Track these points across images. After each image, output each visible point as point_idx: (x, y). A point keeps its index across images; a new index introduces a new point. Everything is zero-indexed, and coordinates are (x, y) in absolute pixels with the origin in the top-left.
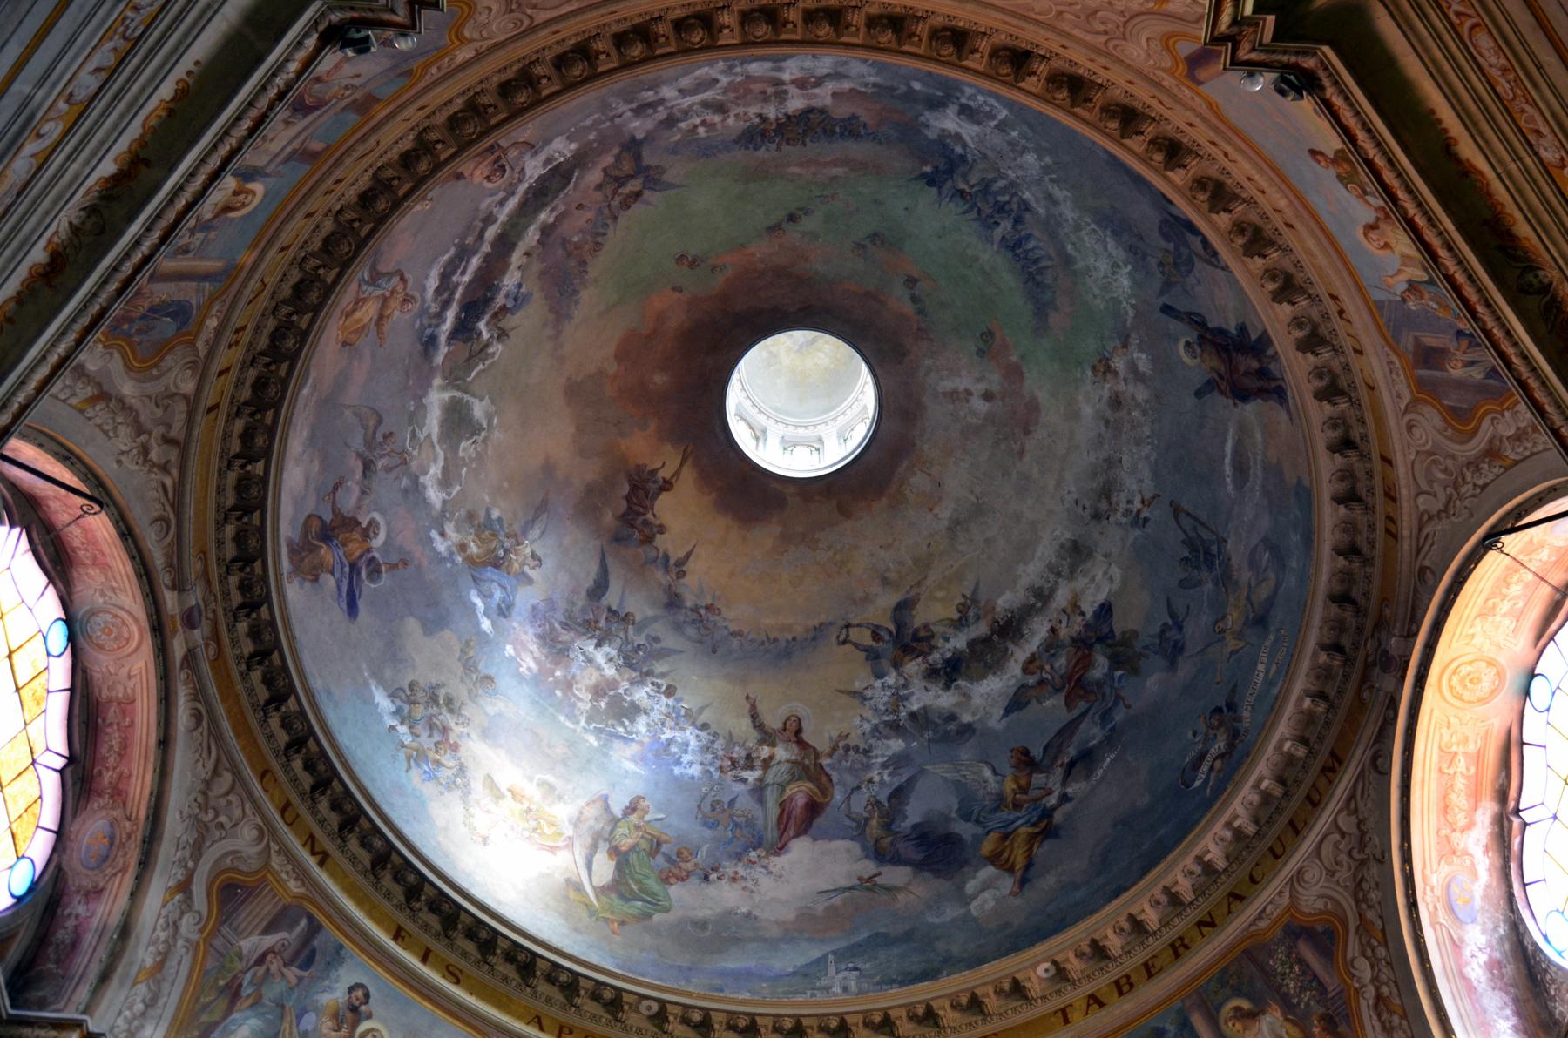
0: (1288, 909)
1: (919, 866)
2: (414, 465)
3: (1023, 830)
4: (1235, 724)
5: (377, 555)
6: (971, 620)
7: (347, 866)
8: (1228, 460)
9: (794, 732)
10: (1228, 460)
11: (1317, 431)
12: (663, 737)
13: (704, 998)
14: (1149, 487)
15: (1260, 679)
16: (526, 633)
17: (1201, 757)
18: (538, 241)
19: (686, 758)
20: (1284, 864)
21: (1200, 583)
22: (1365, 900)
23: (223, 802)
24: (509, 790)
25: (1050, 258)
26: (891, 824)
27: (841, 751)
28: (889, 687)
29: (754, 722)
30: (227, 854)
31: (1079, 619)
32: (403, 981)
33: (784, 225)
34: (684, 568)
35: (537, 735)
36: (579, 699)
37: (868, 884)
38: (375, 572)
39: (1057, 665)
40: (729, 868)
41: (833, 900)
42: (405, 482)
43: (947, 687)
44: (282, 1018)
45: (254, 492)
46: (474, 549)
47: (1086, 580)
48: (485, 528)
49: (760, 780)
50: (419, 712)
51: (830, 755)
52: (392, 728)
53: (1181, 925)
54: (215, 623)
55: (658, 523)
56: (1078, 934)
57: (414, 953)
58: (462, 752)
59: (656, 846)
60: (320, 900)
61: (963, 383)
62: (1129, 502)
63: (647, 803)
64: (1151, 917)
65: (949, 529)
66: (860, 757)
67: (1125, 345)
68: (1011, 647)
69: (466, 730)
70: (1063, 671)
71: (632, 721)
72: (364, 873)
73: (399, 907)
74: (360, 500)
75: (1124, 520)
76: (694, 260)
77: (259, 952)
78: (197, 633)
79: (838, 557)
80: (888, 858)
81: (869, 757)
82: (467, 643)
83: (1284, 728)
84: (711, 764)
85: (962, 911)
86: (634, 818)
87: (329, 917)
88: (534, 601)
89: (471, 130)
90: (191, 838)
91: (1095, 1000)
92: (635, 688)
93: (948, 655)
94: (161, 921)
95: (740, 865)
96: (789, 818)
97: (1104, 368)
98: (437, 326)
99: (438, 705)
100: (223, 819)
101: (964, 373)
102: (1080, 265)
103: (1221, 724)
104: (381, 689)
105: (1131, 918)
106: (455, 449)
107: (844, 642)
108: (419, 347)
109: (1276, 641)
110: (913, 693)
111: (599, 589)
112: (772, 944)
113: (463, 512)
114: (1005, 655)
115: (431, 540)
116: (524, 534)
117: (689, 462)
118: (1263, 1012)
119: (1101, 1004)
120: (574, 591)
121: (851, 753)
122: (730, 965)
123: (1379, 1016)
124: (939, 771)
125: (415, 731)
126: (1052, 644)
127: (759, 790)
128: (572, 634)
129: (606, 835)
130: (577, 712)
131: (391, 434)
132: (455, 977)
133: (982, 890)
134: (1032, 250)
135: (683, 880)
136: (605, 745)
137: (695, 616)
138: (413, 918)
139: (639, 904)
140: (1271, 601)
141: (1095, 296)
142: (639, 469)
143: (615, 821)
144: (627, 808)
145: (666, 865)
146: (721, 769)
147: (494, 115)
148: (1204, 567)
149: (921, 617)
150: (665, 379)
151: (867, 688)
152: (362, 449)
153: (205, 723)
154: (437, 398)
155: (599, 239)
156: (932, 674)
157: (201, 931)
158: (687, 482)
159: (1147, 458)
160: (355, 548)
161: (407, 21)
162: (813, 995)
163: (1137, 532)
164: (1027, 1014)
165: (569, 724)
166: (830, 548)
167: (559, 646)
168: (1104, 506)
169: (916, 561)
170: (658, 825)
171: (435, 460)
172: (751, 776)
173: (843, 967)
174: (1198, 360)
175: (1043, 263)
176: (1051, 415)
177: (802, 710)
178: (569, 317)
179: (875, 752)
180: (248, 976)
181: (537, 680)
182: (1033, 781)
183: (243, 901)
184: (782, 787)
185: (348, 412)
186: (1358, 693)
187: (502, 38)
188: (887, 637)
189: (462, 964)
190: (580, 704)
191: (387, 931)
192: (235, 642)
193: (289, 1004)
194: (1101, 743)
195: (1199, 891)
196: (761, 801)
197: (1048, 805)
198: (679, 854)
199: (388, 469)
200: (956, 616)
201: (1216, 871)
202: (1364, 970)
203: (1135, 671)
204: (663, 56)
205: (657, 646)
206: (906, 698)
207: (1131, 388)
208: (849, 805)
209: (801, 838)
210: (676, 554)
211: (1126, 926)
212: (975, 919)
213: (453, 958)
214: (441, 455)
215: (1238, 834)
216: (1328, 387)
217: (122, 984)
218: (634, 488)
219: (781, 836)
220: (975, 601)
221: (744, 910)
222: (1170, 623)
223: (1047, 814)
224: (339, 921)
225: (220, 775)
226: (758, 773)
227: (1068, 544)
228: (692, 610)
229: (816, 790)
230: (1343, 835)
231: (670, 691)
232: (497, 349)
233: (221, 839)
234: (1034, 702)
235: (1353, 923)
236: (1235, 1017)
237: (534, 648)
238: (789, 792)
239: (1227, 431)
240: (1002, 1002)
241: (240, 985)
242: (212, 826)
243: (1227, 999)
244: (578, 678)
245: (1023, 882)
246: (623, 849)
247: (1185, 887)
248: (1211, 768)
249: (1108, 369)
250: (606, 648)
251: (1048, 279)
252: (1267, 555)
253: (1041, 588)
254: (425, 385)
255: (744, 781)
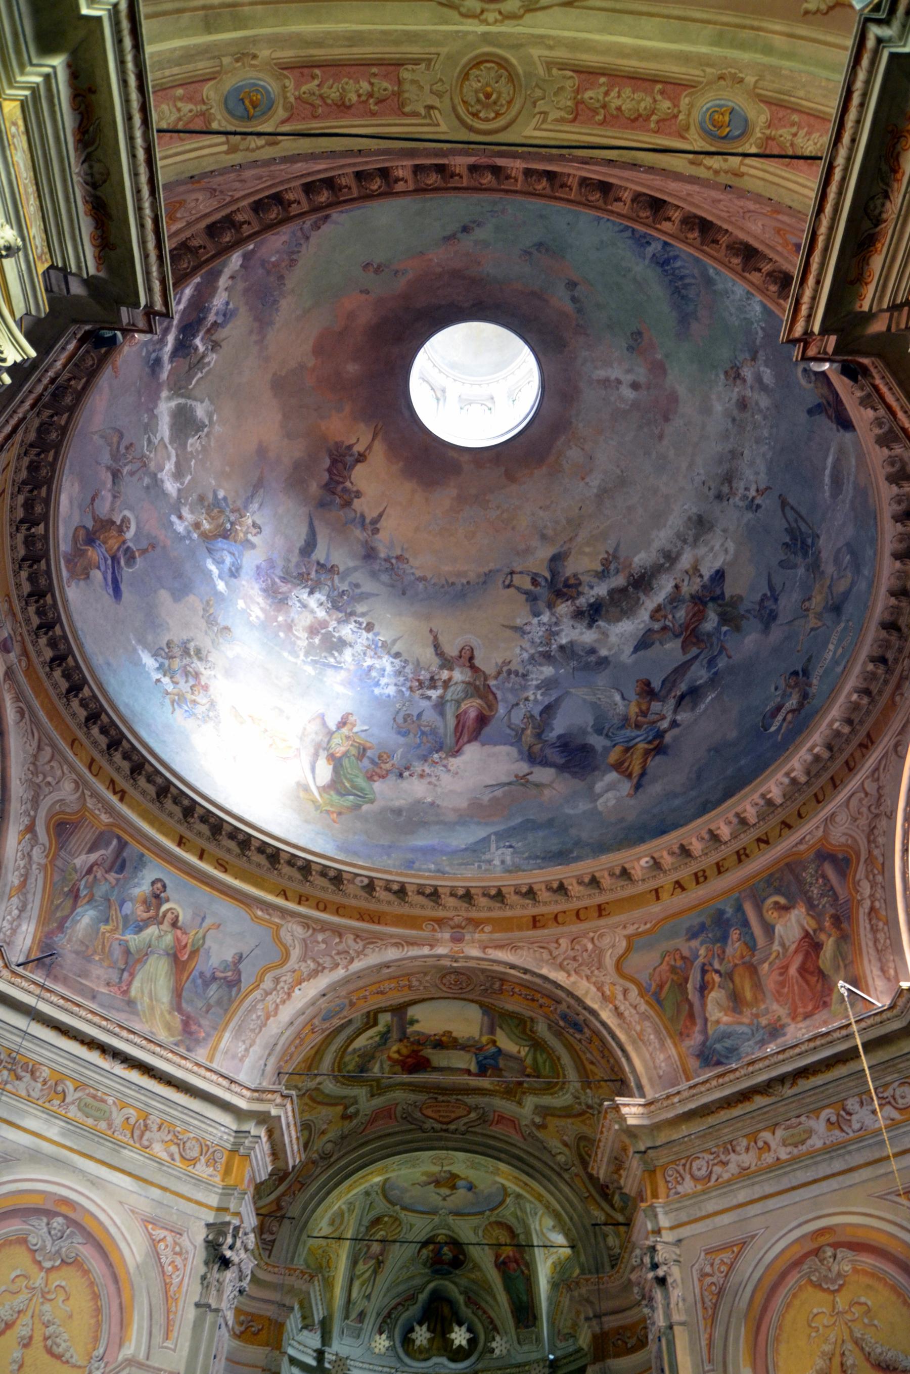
0: (820, 840)
1: (562, 768)
2: (152, 466)
3: (642, 746)
5: (130, 544)
6: (612, 572)
8: (827, 472)
9: (468, 659)
10: (827, 472)
11: (885, 506)
12: (365, 665)
14: (763, 480)
15: (829, 656)
16: (252, 588)
17: (779, 708)
18: (241, 266)
19: (384, 681)
20: (823, 809)
21: (795, 566)
22: (874, 841)
23: (47, 768)
25: (694, 277)
26: (542, 732)
27: (505, 674)
31: (699, 580)
32: (189, 874)
33: (459, 235)
36: (298, 638)
37: (522, 781)
38: (131, 558)
39: (678, 615)
40: (418, 767)
41: (496, 793)
42: (147, 480)
43: (590, 626)
44: (110, 907)
45: (39, 545)
46: (206, 526)
47: (706, 549)
48: (214, 507)
49: (441, 697)
50: (177, 664)
51: (496, 678)
52: (158, 681)
53: (747, 839)
54: (23, 642)
55: (355, 489)
56: (672, 839)
57: (193, 854)
58: (211, 690)
59: (362, 751)
60: (123, 825)
61: (615, 373)
62: (747, 489)
64: (725, 832)
65: (597, 496)
66: (519, 680)
67: (754, 359)
68: (643, 597)
69: (213, 673)
71: (340, 653)
72: (152, 801)
73: (179, 822)
74: (113, 503)
75: (741, 504)
76: (379, 266)
77: (88, 866)
78: (12, 655)
79: (505, 515)
81: (527, 680)
82: (208, 603)
83: (836, 712)
84: (403, 685)
85: (590, 806)
86: (345, 731)
87: (131, 836)
88: (258, 562)
89: (185, 266)
90: (29, 795)
91: (679, 885)
92: (342, 626)
93: (592, 600)
94: (19, 854)
96: (463, 727)
97: (735, 375)
98: (161, 349)
100: (49, 779)
101: (615, 365)
102: (720, 286)
103: (796, 684)
105: (710, 832)
106: (184, 446)
107: (509, 586)
108: (147, 370)
109: (845, 629)
110: (562, 630)
111: (309, 547)
112: (451, 826)
113: (195, 496)
115: (172, 523)
116: (246, 507)
117: (380, 437)
118: (793, 907)
119: (683, 889)
120: (289, 551)
121: (513, 676)
123: (870, 920)
124: (581, 693)
126: (675, 599)
127: (440, 706)
128: (289, 586)
130: (297, 649)
131: (131, 444)
132: (223, 866)
133: (607, 791)
134: (679, 268)
135: (383, 777)
137: (388, 565)
138: (190, 828)
139: (351, 797)
140: (846, 595)
141: (731, 315)
142: (338, 445)
143: (331, 734)
145: (371, 766)
146: (411, 689)
147: (204, 254)
148: (800, 554)
149: (571, 568)
150: (356, 367)
152: (110, 462)
153: (27, 716)
154: (165, 407)
155: (294, 257)
156: (578, 614)
157: (47, 857)
158: (378, 455)
159: (764, 455)
160: (113, 543)
161: (146, 328)
163: (750, 515)
164: (630, 890)
165: (291, 659)
166: (498, 507)
167: (280, 596)
168: (725, 489)
169: (569, 521)
171: (169, 458)
172: (434, 694)
174: (812, 385)
175: (687, 281)
176: (688, 407)
177: (475, 642)
178: (271, 323)
179: (531, 676)
180: (83, 882)
181: (264, 626)
182: (652, 707)
184: (458, 702)
185: (95, 437)
186: (893, 695)
187: (208, 210)
188: (543, 583)
189: (228, 857)
190: (299, 642)
191: (173, 840)
192: (39, 653)
193: (112, 899)
195: (761, 817)
196: (442, 714)
197: (662, 728)
198: (380, 757)
199: (132, 474)
200: (600, 568)
201: (774, 805)
202: (866, 889)
203: (738, 629)
204: (345, 201)
205: (358, 591)
206: (557, 633)
207: (756, 396)
208: (510, 719)
209: (474, 743)
210: (371, 515)
211: (707, 837)
212: (600, 813)
213: (221, 854)
214: (173, 453)
216: (898, 471)
218: (334, 462)
220: (615, 557)
221: (429, 800)
222: (769, 594)
223: (660, 735)
224: (139, 838)
226: (439, 692)
227: (695, 518)
228: (385, 560)
230: (867, 794)
231: (369, 628)
232: (212, 358)
234: (657, 643)
235: (864, 855)
236: (774, 908)
237: (260, 600)
238: (463, 707)
239: (828, 449)
240: (613, 881)
241: (78, 890)
242: (43, 785)
243: (770, 895)
244: (296, 621)
245: (638, 787)
247: (751, 814)
248: (784, 719)
249: (738, 376)
251: (692, 293)
252: (848, 557)
253: (670, 551)
254: (154, 398)
255: (429, 698)
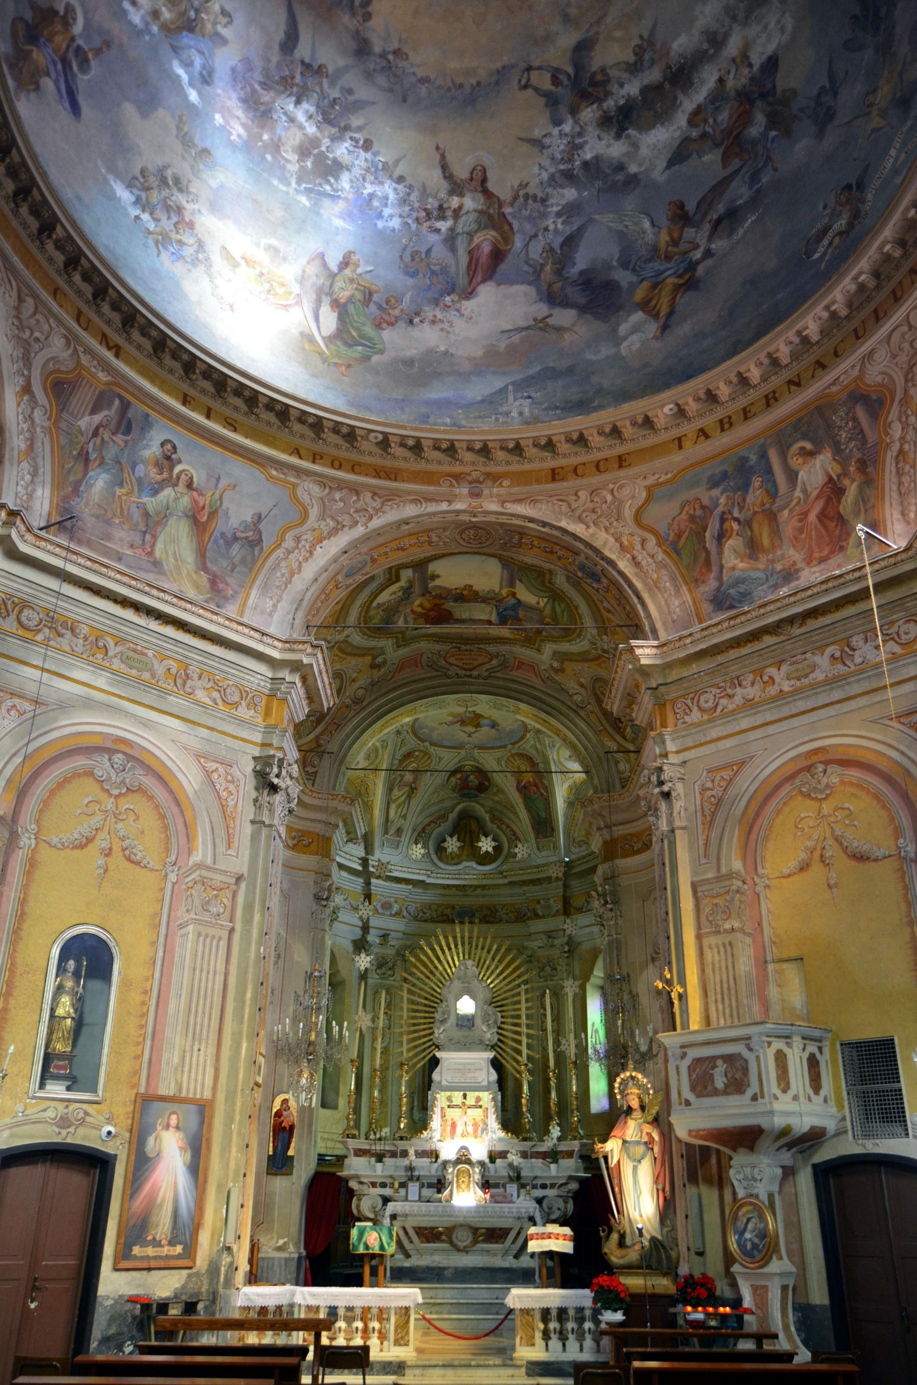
0: (855, 380)
1: (583, 309)
3: (671, 280)
4: (860, 205)
6: (646, 64)
7: (135, 353)
12: (366, 192)
13: (415, 429)
15: (889, 163)
16: (230, 98)
17: (825, 231)
19: (387, 212)
20: (863, 343)
23: (33, 321)
24: (243, 258)
28: (566, 135)
29: (444, 172)
30: (49, 360)
31: (746, 71)
32: (197, 434)
34: (370, 9)
35: (255, 201)
36: (288, 161)
37: (541, 325)
38: (84, 63)
40: (429, 312)
43: (618, 136)
44: (122, 470)
46: (166, 15)
47: (759, 28)
49: (452, 230)
50: (155, 196)
51: (512, 204)
56: (698, 384)
57: (200, 412)
59: (368, 296)
60: (122, 383)
63: (357, 257)
66: (538, 206)
68: (681, 96)
69: (196, 207)
70: (723, 127)
71: (337, 178)
72: (149, 356)
73: (180, 378)
80: (558, 301)
81: (546, 206)
82: (180, 118)
83: (888, 232)
84: (409, 216)
85: (614, 350)
86: (347, 272)
87: (132, 394)
90: (19, 352)
91: (703, 433)
92: (336, 144)
93: (622, 102)
94: (21, 417)
95: (438, 309)
96: (477, 265)
99: (167, 184)
100: (37, 334)
104: (119, 182)
105: (739, 374)
107: (526, 87)
110: (586, 142)
111: (290, 42)
114: (673, 106)
118: (819, 452)
119: (707, 437)
121: (530, 201)
122: (434, 396)
123: (897, 464)
124: (606, 219)
125: (155, 216)
126: (717, 97)
127: (451, 239)
128: (272, 94)
129: (327, 290)
133: (632, 333)
135: (392, 324)
136: (316, 205)
137: (384, 63)
139: (360, 348)
143: (333, 276)
144: (341, 263)
145: (378, 312)
151: (545, 136)
156: (605, 122)
162: (497, 420)
165: (284, 189)
167: (262, 108)
170: (368, 276)
172: (444, 226)
173: (520, 395)
177: (488, 160)
179: (551, 201)
180: (91, 445)
183: (71, 394)
184: (470, 235)
188: (565, 82)
189: (235, 415)
190: (289, 166)
191: (177, 399)
193: (124, 461)
194: (746, 203)
195: (795, 356)
197: (695, 258)
198: (388, 302)
200: (632, 59)
202: (897, 430)
203: (787, 133)
205: (351, 98)
206: (581, 147)
208: (527, 252)
211: (735, 380)
213: (228, 412)
215: (834, 315)
217: (12, 465)
219: (471, 281)
220: (651, 43)
222: (828, 86)
223: (692, 266)
225: (24, 301)
229: (499, 238)
231: (367, 145)
233: (41, 350)
234: (695, 156)
235: (899, 395)
237: (240, 113)
238: (476, 240)
241: (87, 453)
242: (31, 341)
243: (796, 441)
244: (284, 139)
245: (665, 328)
246: (342, 301)
248: (830, 244)
250: (305, 106)
255: (438, 231)
